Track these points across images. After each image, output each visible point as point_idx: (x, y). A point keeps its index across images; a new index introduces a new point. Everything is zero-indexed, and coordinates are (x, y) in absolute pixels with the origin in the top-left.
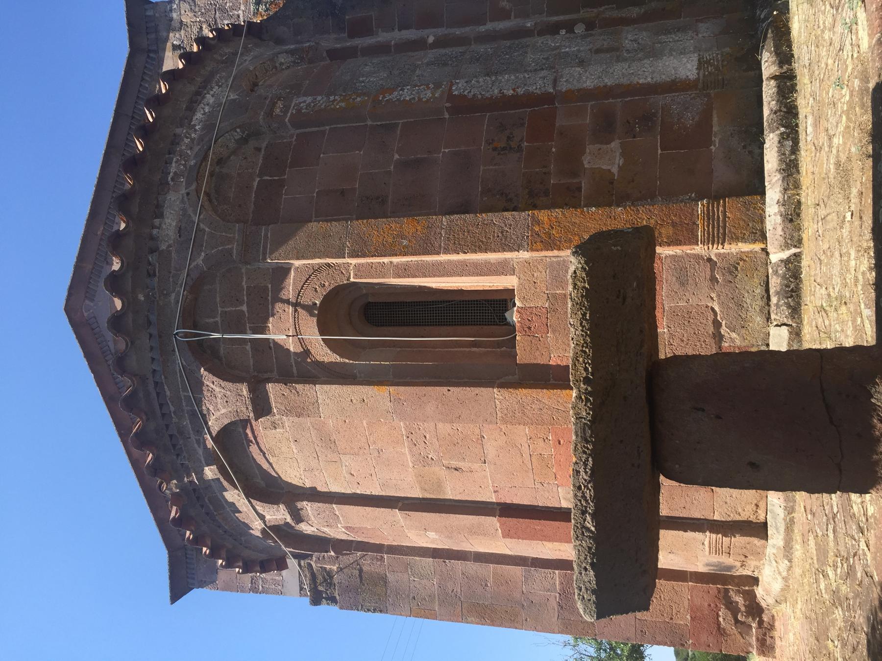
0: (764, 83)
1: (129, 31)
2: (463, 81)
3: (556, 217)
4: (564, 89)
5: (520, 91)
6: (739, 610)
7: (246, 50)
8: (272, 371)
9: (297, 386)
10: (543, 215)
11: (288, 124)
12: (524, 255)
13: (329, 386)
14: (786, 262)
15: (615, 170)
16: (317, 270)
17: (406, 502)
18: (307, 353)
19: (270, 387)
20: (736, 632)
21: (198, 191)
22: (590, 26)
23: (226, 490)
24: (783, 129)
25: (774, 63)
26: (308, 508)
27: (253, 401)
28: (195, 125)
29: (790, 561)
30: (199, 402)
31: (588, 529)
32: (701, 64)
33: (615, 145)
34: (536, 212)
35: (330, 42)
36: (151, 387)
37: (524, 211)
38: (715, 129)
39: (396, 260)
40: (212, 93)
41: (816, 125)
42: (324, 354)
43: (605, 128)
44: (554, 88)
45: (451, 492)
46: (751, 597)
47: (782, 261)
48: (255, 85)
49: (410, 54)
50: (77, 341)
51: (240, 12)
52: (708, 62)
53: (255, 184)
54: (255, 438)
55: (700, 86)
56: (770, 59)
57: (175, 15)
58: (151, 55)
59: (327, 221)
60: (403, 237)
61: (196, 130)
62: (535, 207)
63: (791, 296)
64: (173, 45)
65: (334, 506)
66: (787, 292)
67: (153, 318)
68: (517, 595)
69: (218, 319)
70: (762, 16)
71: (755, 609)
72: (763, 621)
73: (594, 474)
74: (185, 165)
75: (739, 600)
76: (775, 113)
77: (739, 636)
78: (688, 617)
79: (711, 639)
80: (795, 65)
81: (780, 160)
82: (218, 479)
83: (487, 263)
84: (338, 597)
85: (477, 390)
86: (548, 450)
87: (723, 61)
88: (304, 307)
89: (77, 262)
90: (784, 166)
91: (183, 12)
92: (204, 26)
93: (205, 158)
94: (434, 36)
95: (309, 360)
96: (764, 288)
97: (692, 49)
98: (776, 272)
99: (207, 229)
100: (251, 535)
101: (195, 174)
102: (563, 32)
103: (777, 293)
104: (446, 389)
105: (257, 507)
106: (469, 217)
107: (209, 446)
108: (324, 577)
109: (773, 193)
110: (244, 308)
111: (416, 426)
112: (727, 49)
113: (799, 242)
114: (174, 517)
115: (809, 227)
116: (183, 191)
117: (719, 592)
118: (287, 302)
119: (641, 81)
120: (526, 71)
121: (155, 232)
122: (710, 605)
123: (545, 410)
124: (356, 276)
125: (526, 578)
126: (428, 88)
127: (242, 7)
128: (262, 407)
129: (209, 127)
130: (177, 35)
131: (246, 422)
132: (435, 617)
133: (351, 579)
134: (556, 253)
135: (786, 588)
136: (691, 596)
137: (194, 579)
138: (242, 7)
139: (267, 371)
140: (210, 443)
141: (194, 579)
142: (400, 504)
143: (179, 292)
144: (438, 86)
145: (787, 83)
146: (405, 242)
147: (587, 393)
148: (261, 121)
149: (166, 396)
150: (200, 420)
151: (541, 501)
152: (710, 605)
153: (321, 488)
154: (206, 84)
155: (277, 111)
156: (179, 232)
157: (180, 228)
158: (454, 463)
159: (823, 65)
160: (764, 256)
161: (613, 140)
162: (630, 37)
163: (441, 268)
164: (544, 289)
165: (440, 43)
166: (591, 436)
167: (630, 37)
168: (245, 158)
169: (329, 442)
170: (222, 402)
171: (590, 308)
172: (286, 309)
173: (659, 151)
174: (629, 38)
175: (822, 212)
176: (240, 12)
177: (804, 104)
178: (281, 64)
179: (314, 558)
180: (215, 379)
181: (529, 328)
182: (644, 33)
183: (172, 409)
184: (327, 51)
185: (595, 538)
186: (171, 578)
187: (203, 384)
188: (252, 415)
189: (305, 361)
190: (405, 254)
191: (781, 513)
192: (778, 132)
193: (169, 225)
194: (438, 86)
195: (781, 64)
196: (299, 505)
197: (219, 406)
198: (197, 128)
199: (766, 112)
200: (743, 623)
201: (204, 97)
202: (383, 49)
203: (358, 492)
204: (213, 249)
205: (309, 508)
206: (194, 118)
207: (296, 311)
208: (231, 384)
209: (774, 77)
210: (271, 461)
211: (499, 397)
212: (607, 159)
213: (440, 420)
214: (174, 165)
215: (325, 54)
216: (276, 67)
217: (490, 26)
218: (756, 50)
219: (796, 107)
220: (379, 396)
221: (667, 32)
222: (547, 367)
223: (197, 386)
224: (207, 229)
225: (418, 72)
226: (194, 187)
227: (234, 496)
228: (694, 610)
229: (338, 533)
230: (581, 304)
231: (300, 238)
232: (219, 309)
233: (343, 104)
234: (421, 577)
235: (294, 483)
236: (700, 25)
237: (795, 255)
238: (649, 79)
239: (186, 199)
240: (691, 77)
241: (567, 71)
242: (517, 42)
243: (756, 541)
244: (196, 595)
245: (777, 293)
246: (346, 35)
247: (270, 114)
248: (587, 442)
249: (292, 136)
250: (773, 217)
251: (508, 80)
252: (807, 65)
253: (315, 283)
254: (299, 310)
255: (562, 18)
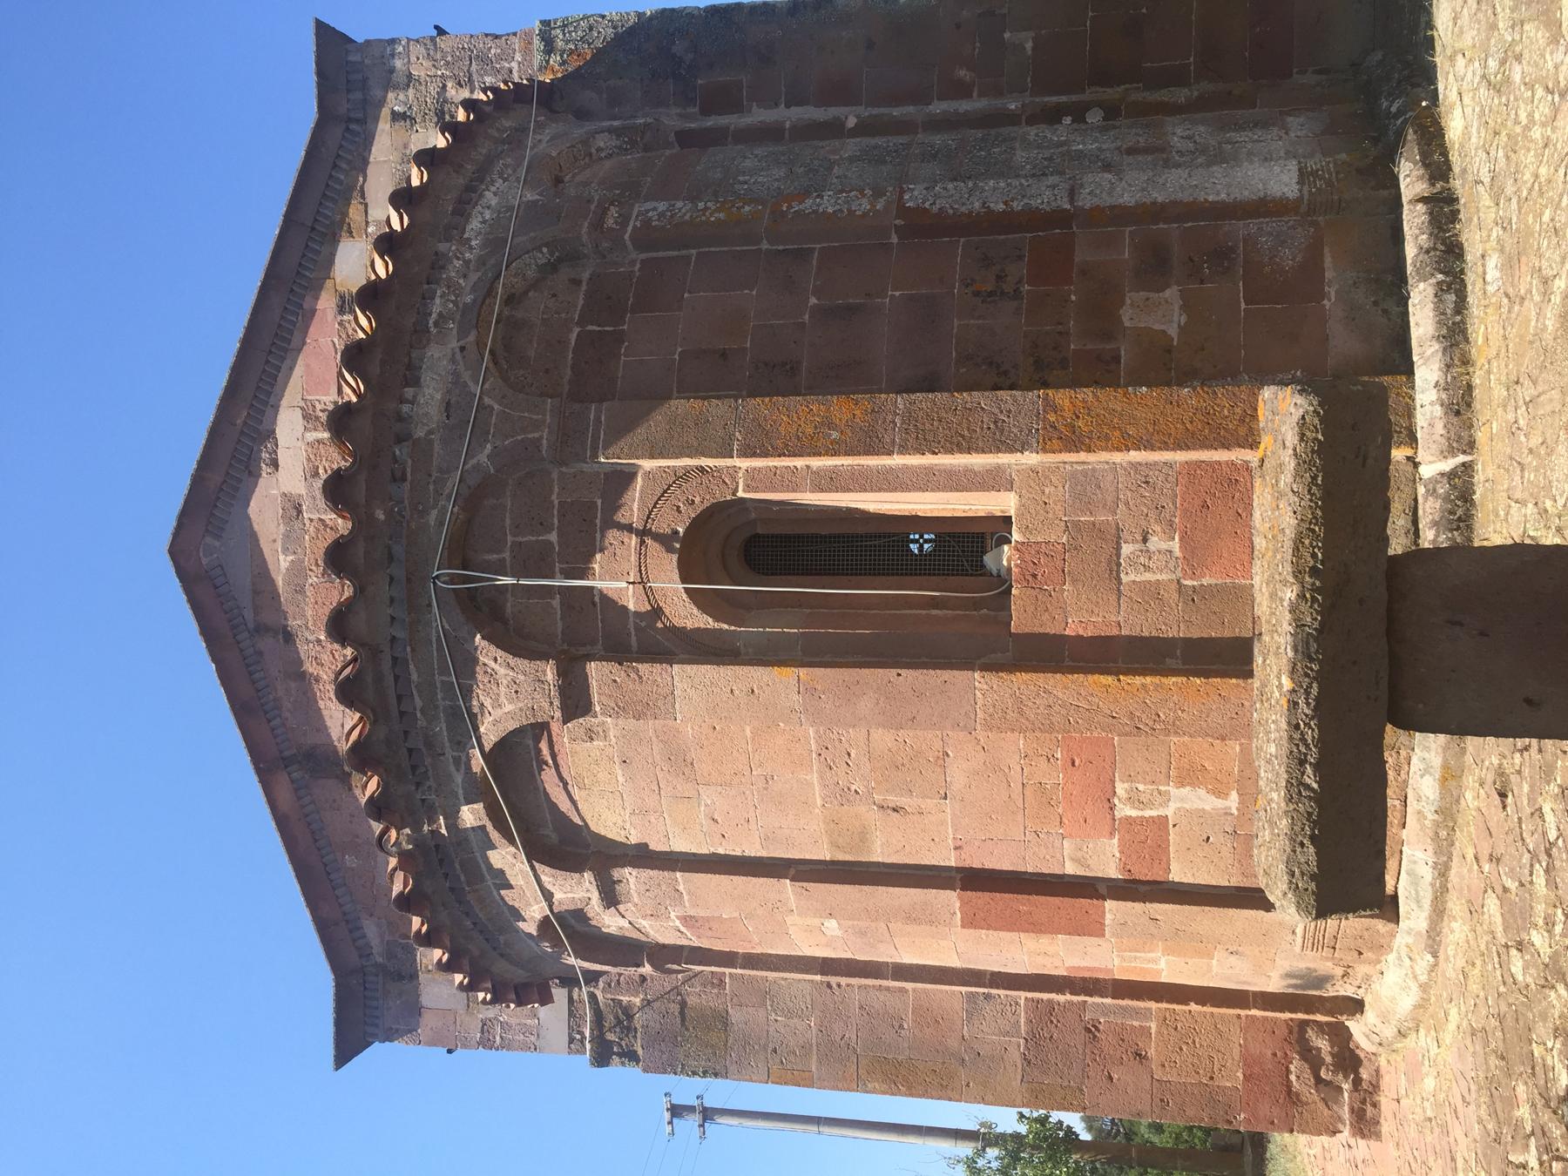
0: (1406, 207)
1: (319, 85)
2: (921, 187)
3: (1083, 401)
4: (1088, 206)
5: (1017, 206)
6: (1322, 1062)
7: (540, 126)
8: (593, 642)
9: (640, 666)
10: (1062, 397)
11: (628, 243)
12: (1031, 459)
13: (695, 667)
14: (1451, 476)
15: (1173, 331)
16: (684, 476)
17: (801, 867)
18: (657, 612)
19: (593, 668)
20: (1317, 1099)
21: (480, 345)
22: (1112, 112)
23: (493, 847)
24: (1440, 277)
25: (1420, 178)
26: (631, 879)
27: (564, 692)
28: (469, 239)
29: (1435, 956)
30: (467, 693)
31: (1308, 787)
32: (1303, 176)
33: (1172, 293)
34: (1050, 392)
35: (672, 119)
36: (386, 665)
37: (1030, 389)
38: (1329, 275)
39: (816, 463)
40: (493, 189)
41: (1510, 265)
42: (685, 614)
43: (1155, 267)
44: (1072, 201)
45: (879, 853)
46: (1340, 1036)
47: (1442, 475)
48: (558, 181)
49: (816, 143)
50: (188, 606)
51: (514, 65)
52: (1314, 173)
53: (573, 337)
54: (554, 756)
55: (1304, 208)
56: (1415, 173)
57: (398, 63)
58: (353, 126)
59: (704, 398)
60: (831, 425)
61: (471, 248)
62: (1045, 385)
63: (1458, 528)
64: (393, 113)
65: (678, 874)
66: (1450, 522)
67: (398, 550)
68: (953, 1043)
69: (507, 555)
70: (1393, 109)
71: (1348, 1060)
72: (1361, 1079)
73: (1320, 708)
74: (455, 303)
75: (1322, 1044)
76: (1427, 252)
77: (1321, 1105)
78: (1240, 1075)
79: (1276, 1111)
80: (1456, 184)
81: (1439, 322)
82: (483, 828)
83: (968, 471)
84: (640, 1052)
85: (947, 675)
86: (1054, 776)
87: (1337, 173)
88: (658, 537)
89: (197, 470)
90: (1444, 331)
91: (413, 59)
92: (449, 85)
93: (490, 292)
94: (857, 117)
95: (660, 625)
96: (1410, 518)
97: (1282, 154)
98: (1432, 492)
99: (496, 407)
100: (517, 931)
101: (473, 317)
102: (1067, 120)
103: (1435, 524)
104: (894, 671)
105: (543, 878)
106: (941, 397)
107: (476, 769)
108: (617, 1017)
109: (1428, 372)
110: (553, 537)
111: (835, 736)
112: (1343, 156)
113: (1471, 446)
114: (401, 894)
115: (1490, 424)
116: (454, 344)
117: (1291, 1032)
118: (629, 528)
119: (1210, 198)
120: (1017, 176)
121: (405, 408)
122: (1275, 1055)
123: (1057, 708)
124: (748, 488)
125: (970, 1014)
126: (864, 196)
127: (518, 57)
128: (575, 703)
129: (494, 243)
130: (402, 97)
131: (540, 729)
132: (810, 1084)
133: (668, 1018)
134: (1082, 456)
135: (1421, 1006)
136: (1245, 1039)
137: (377, 1026)
138: (518, 57)
139: (585, 640)
140: (478, 762)
141: (377, 1026)
142: (792, 872)
143: (445, 508)
144: (878, 193)
145: (1443, 209)
146: (835, 435)
147: (1314, 589)
148: (585, 238)
149: (409, 681)
150: (464, 722)
151: (1031, 865)
152: (1275, 1055)
153: (655, 846)
154: (482, 175)
155: (610, 222)
156: (447, 410)
157: (448, 404)
158: (893, 800)
159: (1528, 176)
160: (1410, 468)
161: (1168, 286)
162: (1179, 131)
163: (890, 478)
164: (1061, 515)
165: (863, 129)
166: (1317, 652)
167: (1179, 131)
168: (554, 295)
169: (680, 761)
170: (506, 692)
171: (1323, 469)
172: (626, 540)
173: (1243, 306)
174: (1178, 133)
175: (1527, 391)
176: (514, 65)
177: (1477, 239)
178: (599, 150)
179: (601, 985)
180: (500, 653)
181: (1034, 576)
182: (1202, 129)
183: (419, 703)
184: (676, 133)
185: (1318, 798)
186: (339, 1023)
187: (476, 661)
188: (558, 714)
189: (652, 626)
190: (835, 454)
191: (1427, 874)
192: (1433, 281)
193: (430, 396)
194: (878, 193)
195: (1433, 180)
196: (617, 873)
197: (503, 699)
198: (473, 243)
199: (1410, 251)
200: (1328, 1083)
201: (481, 196)
202: (772, 133)
203: (721, 851)
204: (507, 438)
205: (632, 880)
206: (468, 228)
207: (642, 542)
208: (526, 662)
209: (1423, 200)
210: (576, 798)
211: (983, 687)
212: (1161, 313)
213: (879, 725)
214: (438, 301)
215: (672, 138)
216: (591, 155)
217: (938, 107)
218: (1390, 157)
219: (1460, 246)
220: (780, 684)
221: (1240, 128)
222: (1061, 639)
223: (467, 665)
224: (496, 407)
225: (836, 170)
226: (472, 338)
227: (506, 857)
228: (1248, 1061)
229: (664, 931)
230: (1311, 463)
231: (658, 421)
232: (509, 538)
233: (722, 215)
234: (790, 1014)
235: (610, 836)
236: (1290, 119)
237: (1463, 464)
238: (1223, 196)
239: (458, 356)
240: (1291, 195)
241: (1089, 178)
242: (993, 132)
243: (1380, 926)
244: (377, 1051)
245: (1435, 524)
246: (696, 109)
247: (598, 225)
248: (1311, 660)
249: (633, 262)
250: (1428, 408)
251: (995, 189)
252: (1487, 180)
253: (677, 496)
254: (649, 541)
255: (1064, 99)
